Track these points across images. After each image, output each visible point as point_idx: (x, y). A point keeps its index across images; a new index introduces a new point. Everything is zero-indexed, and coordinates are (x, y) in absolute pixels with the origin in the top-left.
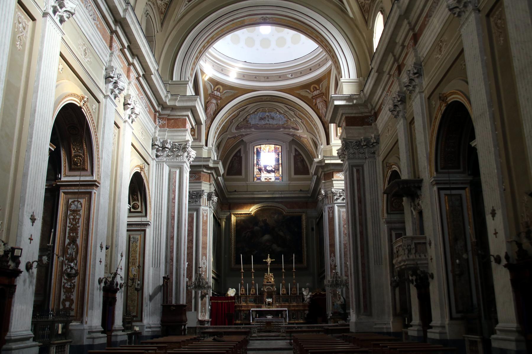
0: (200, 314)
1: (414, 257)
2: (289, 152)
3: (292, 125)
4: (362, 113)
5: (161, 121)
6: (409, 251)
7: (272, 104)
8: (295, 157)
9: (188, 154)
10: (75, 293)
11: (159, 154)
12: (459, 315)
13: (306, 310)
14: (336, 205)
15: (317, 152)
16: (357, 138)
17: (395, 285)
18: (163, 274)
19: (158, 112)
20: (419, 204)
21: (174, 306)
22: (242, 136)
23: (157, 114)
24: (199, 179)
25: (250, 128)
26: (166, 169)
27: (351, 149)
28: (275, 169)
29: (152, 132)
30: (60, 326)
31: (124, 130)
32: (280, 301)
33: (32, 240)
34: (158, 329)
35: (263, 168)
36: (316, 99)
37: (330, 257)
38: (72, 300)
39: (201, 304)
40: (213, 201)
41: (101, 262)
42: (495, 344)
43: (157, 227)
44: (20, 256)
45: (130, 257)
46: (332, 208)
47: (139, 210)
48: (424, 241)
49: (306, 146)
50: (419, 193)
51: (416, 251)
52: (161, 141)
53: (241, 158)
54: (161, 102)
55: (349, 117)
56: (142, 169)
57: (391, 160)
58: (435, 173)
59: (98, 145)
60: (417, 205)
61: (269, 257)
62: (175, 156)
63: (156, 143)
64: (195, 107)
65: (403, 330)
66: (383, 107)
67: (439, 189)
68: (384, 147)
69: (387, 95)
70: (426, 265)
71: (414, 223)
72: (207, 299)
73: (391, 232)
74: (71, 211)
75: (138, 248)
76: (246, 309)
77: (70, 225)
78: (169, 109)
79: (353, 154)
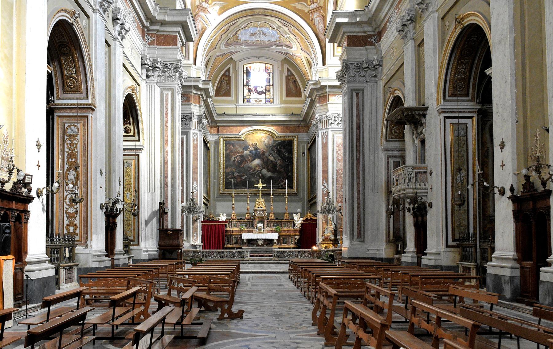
0: (191, 238)
1: (414, 187)
2: (281, 72)
3: (285, 43)
4: (365, 32)
5: (149, 38)
6: (410, 180)
7: (262, 18)
8: (287, 77)
9: (180, 74)
10: (78, 218)
11: (149, 73)
12: (455, 244)
13: (297, 235)
14: (330, 130)
15: (311, 73)
16: (358, 60)
17: (390, 213)
18: (158, 200)
19: (147, 27)
20: (421, 133)
21: (170, 230)
22: (231, 53)
23: (145, 29)
24: (188, 100)
25: (241, 44)
26: (158, 90)
27: (351, 72)
28: (266, 90)
29: (141, 50)
30: (67, 249)
31: (115, 48)
32: (270, 227)
33: (37, 165)
34: (156, 253)
35: (253, 89)
36: (313, 14)
37: (323, 183)
38: (76, 225)
39: (193, 228)
40: (203, 124)
41: (101, 187)
42: (489, 271)
43: (151, 152)
44: (31, 183)
45: (125, 182)
46: (326, 133)
47: (132, 134)
48: (425, 171)
49: (299, 65)
50: (423, 120)
51: (416, 180)
52: (151, 59)
53: (229, 78)
54: (149, 17)
55: (350, 36)
56: (133, 90)
57: (395, 84)
58: (442, 101)
59: (91, 65)
60: (420, 133)
61: (260, 182)
62: (166, 77)
63: (146, 63)
64: (186, 22)
65: (396, 256)
66: (389, 26)
67: (445, 118)
68: (386, 71)
69: (395, 12)
70: (426, 194)
71: (415, 152)
72: (199, 225)
73: (388, 159)
74: (67, 136)
75: (132, 173)
76: (237, 233)
77: (68, 150)
78: (157, 24)
79: (353, 77)
